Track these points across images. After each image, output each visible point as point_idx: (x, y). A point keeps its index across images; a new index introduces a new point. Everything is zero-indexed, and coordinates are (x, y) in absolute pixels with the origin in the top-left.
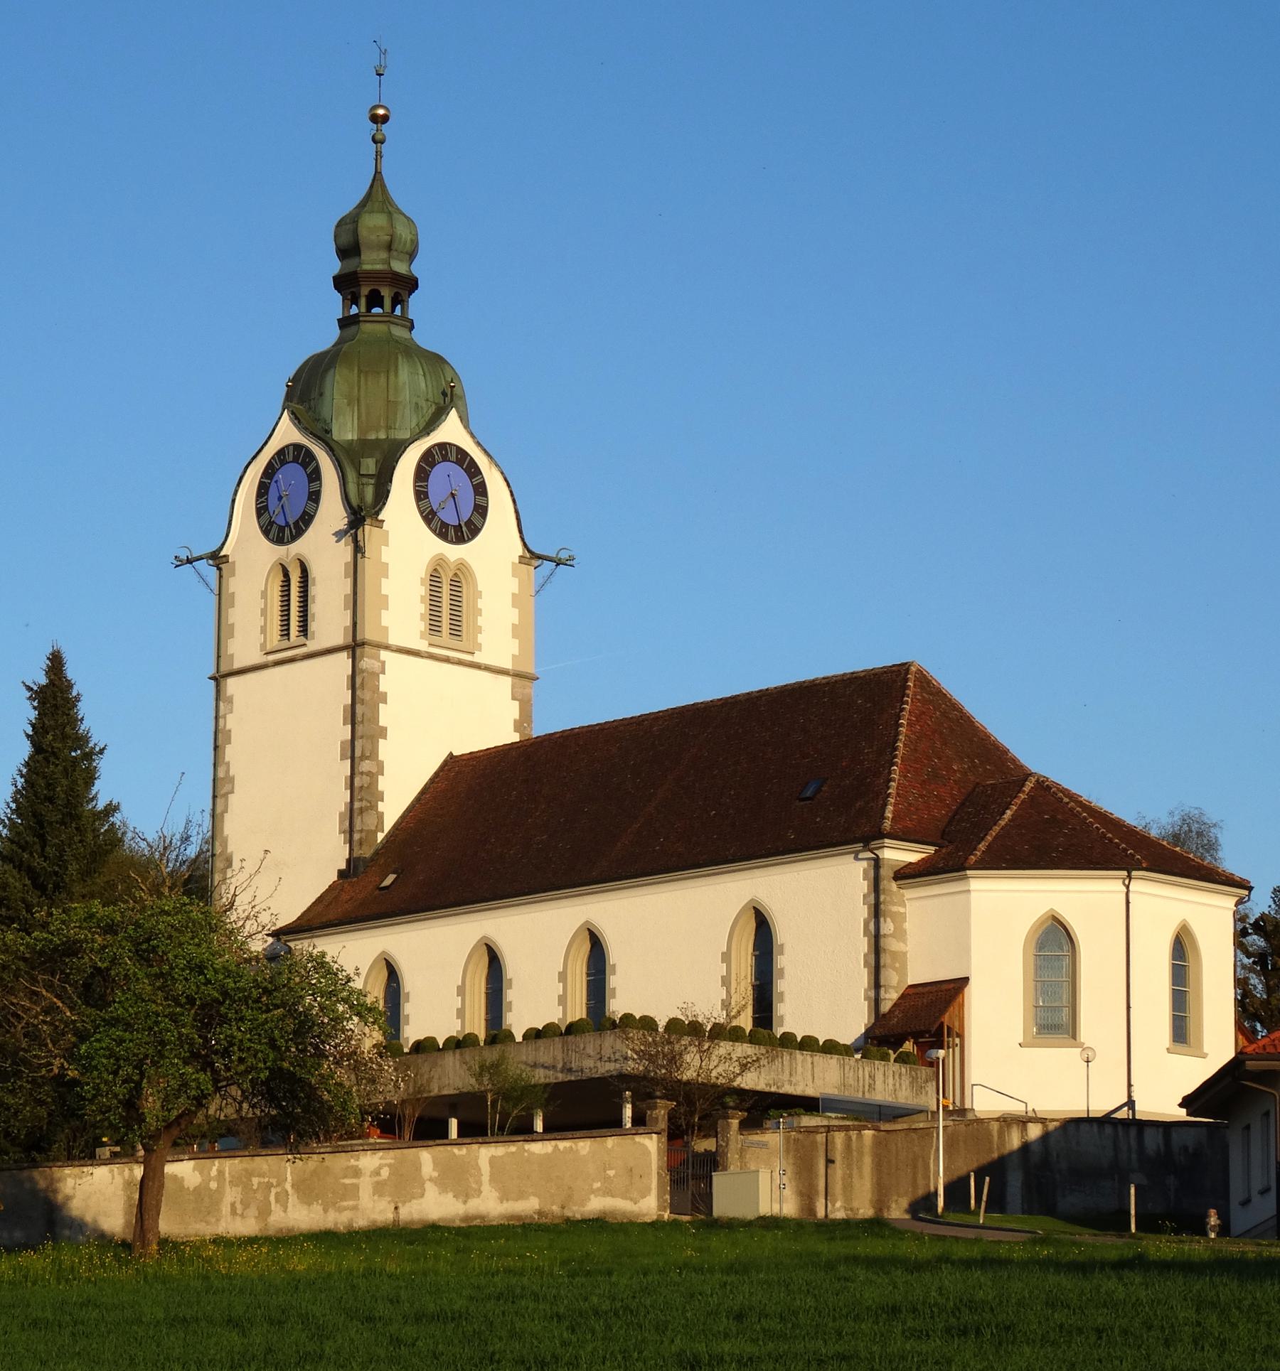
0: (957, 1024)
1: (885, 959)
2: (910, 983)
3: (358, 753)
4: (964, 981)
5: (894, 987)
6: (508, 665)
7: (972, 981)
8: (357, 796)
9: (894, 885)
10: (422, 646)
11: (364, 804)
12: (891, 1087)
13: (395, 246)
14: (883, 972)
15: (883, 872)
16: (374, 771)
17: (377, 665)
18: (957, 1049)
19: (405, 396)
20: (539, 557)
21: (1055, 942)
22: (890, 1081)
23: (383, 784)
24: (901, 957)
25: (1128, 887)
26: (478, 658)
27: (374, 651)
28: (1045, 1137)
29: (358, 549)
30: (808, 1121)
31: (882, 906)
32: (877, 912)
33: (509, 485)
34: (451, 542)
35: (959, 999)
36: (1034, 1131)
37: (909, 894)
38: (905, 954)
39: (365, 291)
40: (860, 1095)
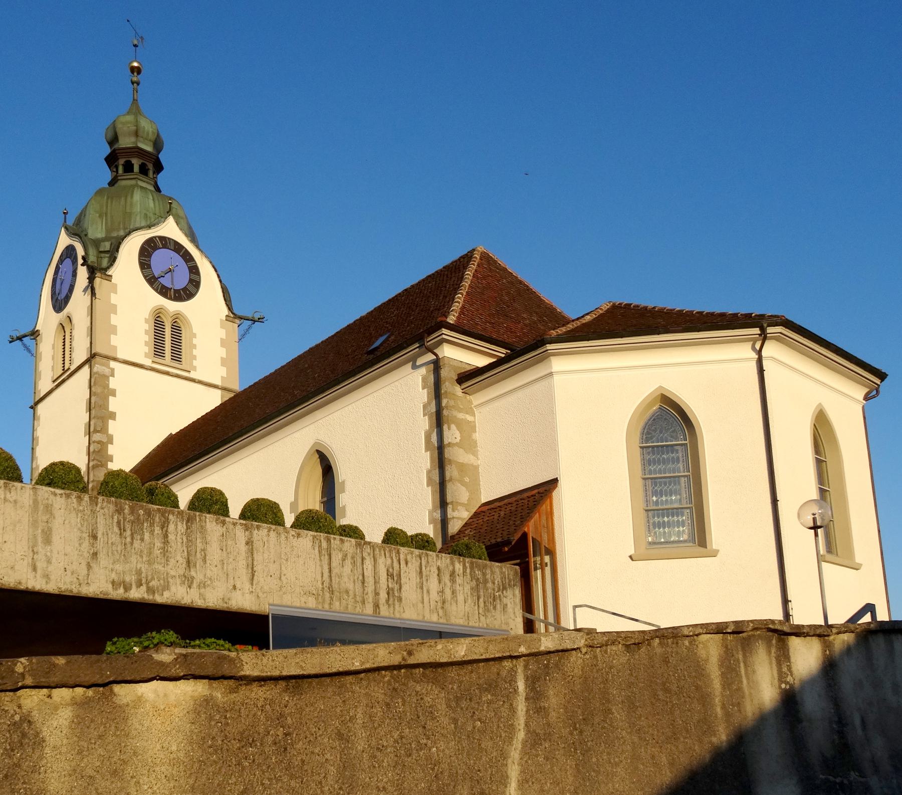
1: (451, 472)
2: (484, 500)
3: (92, 430)
5: (462, 504)
6: (218, 382)
7: (562, 483)
8: (92, 458)
9: (458, 390)
10: (148, 362)
11: (95, 462)
12: (434, 595)
13: (140, 133)
14: (450, 488)
15: (444, 373)
16: (105, 441)
17: (107, 371)
18: (548, 570)
19: (137, 208)
20: (241, 318)
21: (668, 429)
22: (433, 584)
23: (111, 450)
26: (192, 375)
27: (105, 360)
29: (93, 294)
30: (250, 661)
31: (445, 412)
32: (439, 421)
33: (216, 271)
34: (170, 299)
35: (544, 508)
36: (806, 658)
37: (477, 399)
38: (476, 468)
39: (121, 161)
40: (369, 609)
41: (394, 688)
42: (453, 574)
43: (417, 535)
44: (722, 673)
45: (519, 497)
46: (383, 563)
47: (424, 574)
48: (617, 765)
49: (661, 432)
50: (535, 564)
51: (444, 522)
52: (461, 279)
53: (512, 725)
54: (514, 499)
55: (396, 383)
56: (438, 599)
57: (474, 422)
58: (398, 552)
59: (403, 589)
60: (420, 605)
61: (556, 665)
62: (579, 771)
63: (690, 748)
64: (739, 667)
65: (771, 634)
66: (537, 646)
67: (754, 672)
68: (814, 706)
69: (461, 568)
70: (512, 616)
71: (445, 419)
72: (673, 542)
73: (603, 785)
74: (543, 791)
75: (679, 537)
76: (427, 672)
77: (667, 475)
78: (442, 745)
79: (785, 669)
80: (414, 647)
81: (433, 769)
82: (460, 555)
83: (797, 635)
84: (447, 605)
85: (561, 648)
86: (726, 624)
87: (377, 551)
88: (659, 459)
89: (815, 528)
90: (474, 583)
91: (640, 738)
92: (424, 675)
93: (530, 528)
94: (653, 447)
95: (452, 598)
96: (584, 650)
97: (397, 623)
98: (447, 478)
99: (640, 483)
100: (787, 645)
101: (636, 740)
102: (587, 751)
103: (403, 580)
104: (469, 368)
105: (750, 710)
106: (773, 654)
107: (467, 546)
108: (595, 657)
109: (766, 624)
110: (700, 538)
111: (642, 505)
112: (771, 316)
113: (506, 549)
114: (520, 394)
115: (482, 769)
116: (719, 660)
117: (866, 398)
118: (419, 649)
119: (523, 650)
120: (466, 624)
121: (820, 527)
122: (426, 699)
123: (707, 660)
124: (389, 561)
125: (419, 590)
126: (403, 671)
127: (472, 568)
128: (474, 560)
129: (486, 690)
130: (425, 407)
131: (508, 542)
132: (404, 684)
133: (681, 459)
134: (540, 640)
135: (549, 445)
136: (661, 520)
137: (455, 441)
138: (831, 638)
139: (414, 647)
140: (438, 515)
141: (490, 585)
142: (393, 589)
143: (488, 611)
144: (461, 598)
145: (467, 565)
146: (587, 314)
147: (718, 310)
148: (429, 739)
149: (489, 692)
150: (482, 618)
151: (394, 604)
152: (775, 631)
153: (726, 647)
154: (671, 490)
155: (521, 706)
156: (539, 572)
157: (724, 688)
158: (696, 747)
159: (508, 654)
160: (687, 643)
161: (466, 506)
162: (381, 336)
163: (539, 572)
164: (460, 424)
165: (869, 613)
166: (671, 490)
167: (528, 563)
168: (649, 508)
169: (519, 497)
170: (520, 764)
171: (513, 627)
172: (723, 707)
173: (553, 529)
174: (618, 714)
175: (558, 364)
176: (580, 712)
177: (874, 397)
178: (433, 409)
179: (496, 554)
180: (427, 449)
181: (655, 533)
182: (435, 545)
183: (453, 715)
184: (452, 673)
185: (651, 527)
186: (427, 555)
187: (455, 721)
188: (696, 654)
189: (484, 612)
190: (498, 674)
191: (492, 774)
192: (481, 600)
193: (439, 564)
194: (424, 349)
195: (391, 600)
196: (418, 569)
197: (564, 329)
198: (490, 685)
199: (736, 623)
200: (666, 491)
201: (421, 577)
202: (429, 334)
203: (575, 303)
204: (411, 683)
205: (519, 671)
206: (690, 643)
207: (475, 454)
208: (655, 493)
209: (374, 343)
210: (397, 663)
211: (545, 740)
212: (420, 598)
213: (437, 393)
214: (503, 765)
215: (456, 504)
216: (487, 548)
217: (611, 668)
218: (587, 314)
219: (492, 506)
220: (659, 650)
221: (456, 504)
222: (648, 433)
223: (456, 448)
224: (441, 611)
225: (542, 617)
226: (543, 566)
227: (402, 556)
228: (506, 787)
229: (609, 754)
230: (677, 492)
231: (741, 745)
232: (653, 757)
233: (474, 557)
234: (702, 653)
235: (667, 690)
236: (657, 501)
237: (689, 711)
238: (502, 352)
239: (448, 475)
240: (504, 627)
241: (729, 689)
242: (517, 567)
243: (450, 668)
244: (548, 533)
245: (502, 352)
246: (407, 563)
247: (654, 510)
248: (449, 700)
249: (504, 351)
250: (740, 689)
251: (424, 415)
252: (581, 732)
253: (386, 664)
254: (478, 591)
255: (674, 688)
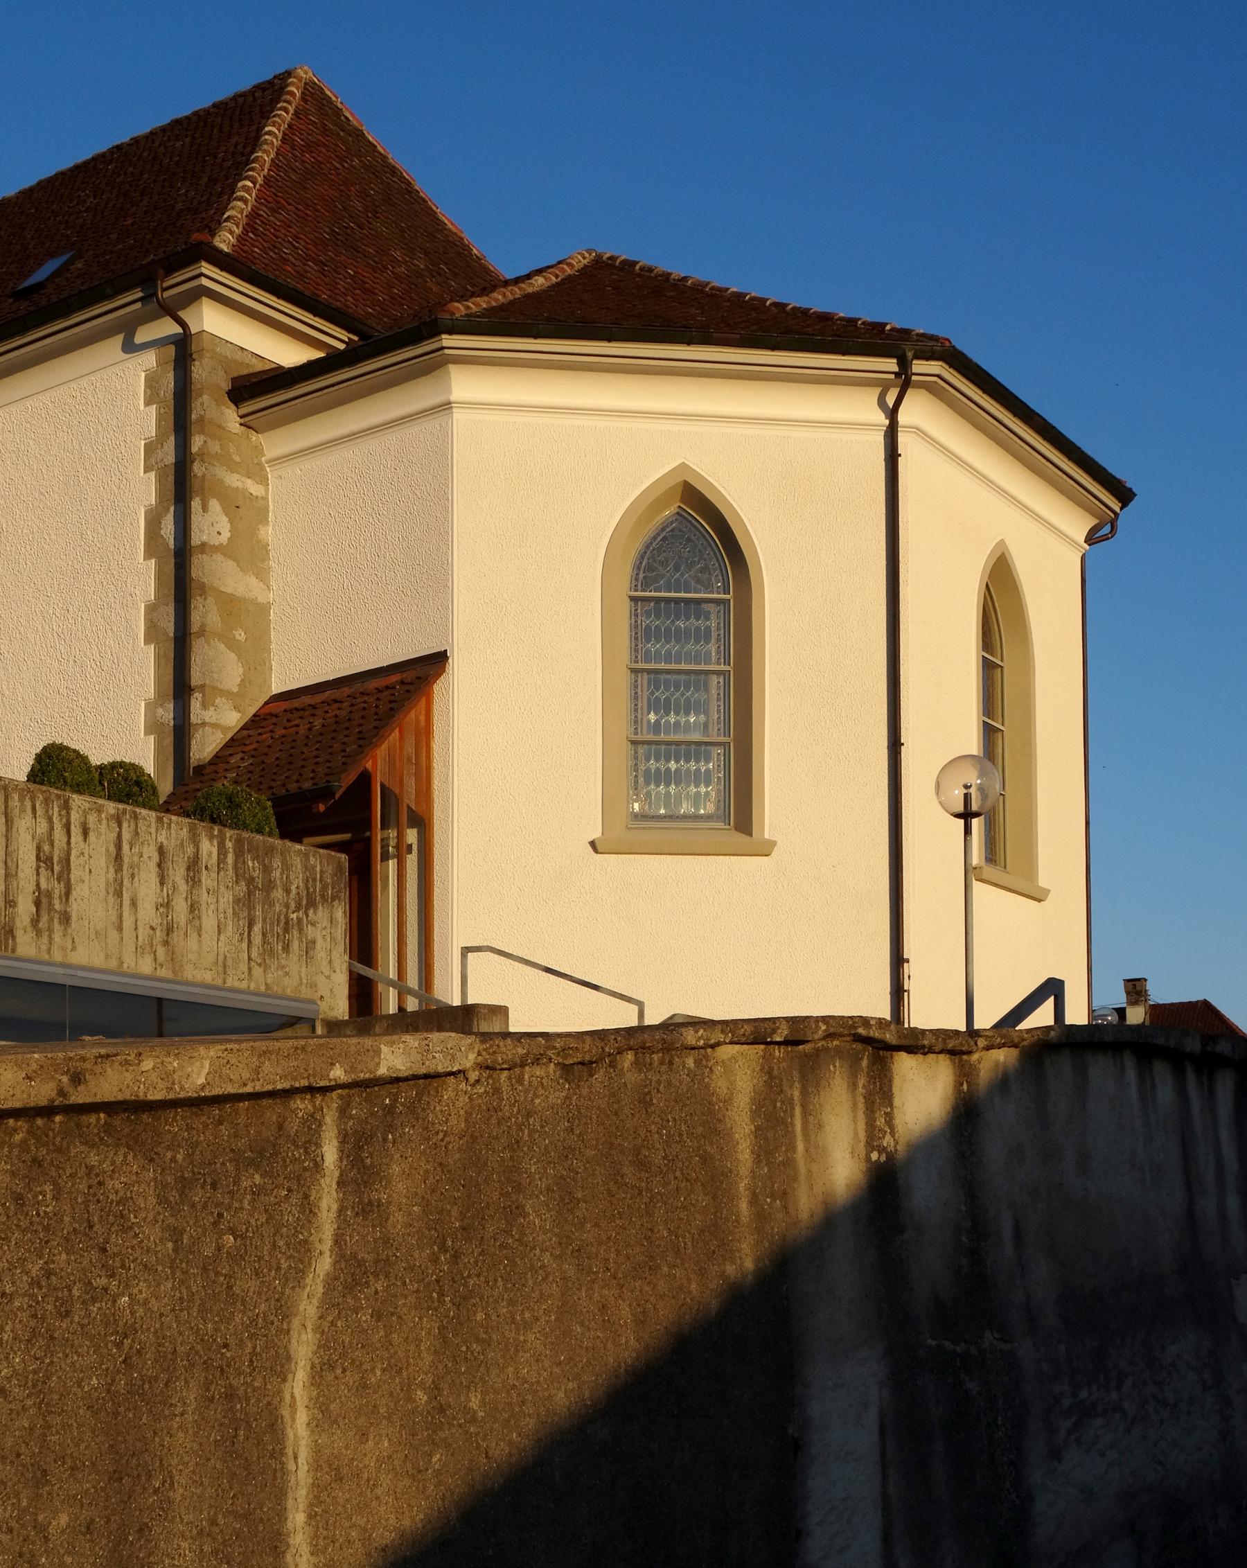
0: (410, 784)
1: (204, 613)
2: (276, 688)
4: (436, 662)
7: (458, 667)
9: (231, 417)
12: (148, 913)
14: (200, 653)
15: (200, 371)
18: (412, 861)
21: (690, 563)
22: (147, 887)
24: (252, 616)
25: (892, 414)
28: (966, 1114)
31: (197, 469)
32: (181, 486)
35: (413, 716)
36: (923, 1097)
37: (275, 444)
38: (264, 609)
41: (34, 1160)
42: (193, 865)
43: (114, 766)
44: (758, 1128)
45: (358, 687)
46: (27, 830)
47: (126, 860)
48: (527, 1326)
49: (677, 569)
50: (385, 847)
51: (181, 733)
52: (254, 141)
53: (306, 1241)
54: (346, 691)
55: (84, 382)
56: (156, 921)
57: (265, 499)
58: (66, 807)
59: (74, 894)
60: (113, 935)
61: (411, 1109)
62: (445, 1340)
63: (680, 1288)
64: (792, 1116)
65: (858, 1046)
66: (372, 1065)
67: (820, 1126)
68: (928, 1196)
69: (215, 851)
70: (324, 967)
71: (196, 485)
72: (685, 817)
73: (495, 1372)
74: (366, 1387)
75: (697, 806)
76: (117, 1121)
77: (683, 666)
78: (142, 1289)
79: (880, 1122)
80: (88, 1065)
81: (119, 1345)
82: (213, 820)
83: (910, 1050)
84: (176, 937)
85: (423, 1071)
86: (772, 1022)
87: (15, 801)
88: (668, 630)
89: (966, 815)
90: (242, 888)
91: (580, 1268)
92: (108, 1128)
93: (378, 763)
94: (658, 600)
95: (190, 921)
96: (473, 1076)
97: (57, 975)
98: (195, 628)
99: (623, 679)
100: (890, 1070)
101: (570, 1270)
102: (465, 1298)
103: (75, 873)
104: (259, 367)
105: (806, 1205)
106: (861, 1090)
107: (230, 799)
108: (497, 1090)
109: (853, 1027)
110: (740, 813)
111: (623, 729)
112: (923, 335)
113: (322, 808)
114: (373, 444)
115: (232, 1341)
116: (753, 1101)
117: (1091, 539)
118: (98, 1069)
119: (338, 1073)
120: (219, 982)
121: (977, 815)
122: (110, 1184)
123: (728, 1101)
124: (42, 827)
125: (111, 899)
126: (58, 1119)
127: (239, 853)
128: (245, 835)
129: (251, 1163)
130: (149, 449)
131: (327, 793)
132: (59, 1150)
133: (714, 634)
134: (378, 1052)
135: (432, 574)
136: (662, 765)
137: (216, 541)
138: (975, 1057)
139: (88, 1065)
140: (167, 714)
141: (278, 894)
142: (49, 894)
143: (272, 953)
144: (209, 921)
145: (229, 845)
146: (539, 272)
147: (818, 305)
148: (112, 1276)
149: (257, 1168)
150: (257, 971)
151: (50, 930)
152: (867, 1040)
153: (770, 1073)
154: (688, 701)
155: (328, 1200)
156: (392, 864)
157: (757, 1161)
158: (694, 1286)
159: (305, 1083)
160: (690, 1062)
161: (236, 700)
162: (52, 257)
163: (392, 864)
164: (234, 504)
165: (1051, 1000)
166: (688, 701)
167: (368, 843)
168: (639, 737)
169: (358, 687)
170: (318, 1329)
171: (326, 994)
172: (754, 1200)
173: (429, 769)
174: (538, 1215)
175: (464, 385)
176: (455, 1212)
177: (1105, 538)
178: (168, 454)
179: (295, 820)
180: (148, 554)
181: (648, 794)
182: (154, 790)
183: (171, 1220)
184: (175, 1124)
185: (641, 780)
186: (135, 817)
187: (176, 1234)
188: (707, 1087)
189: (262, 955)
190: (280, 1127)
191: (254, 1353)
192: (257, 929)
193: (162, 838)
194: (153, 306)
195: (44, 918)
196: (112, 849)
197: (483, 302)
198: (261, 1153)
199: (793, 1021)
200: (677, 701)
201: (119, 869)
202: (170, 271)
203: (518, 243)
204: (77, 1148)
205: (328, 1120)
206: (698, 1062)
207: (263, 575)
208: (654, 705)
209: (31, 272)
210: (43, 1102)
211: (376, 1276)
212: (114, 918)
213: (180, 417)
214: (280, 1331)
215: (212, 693)
216: (277, 802)
217: (529, 1115)
218: (539, 272)
219: (296, 703)
220: (632, 1078)
221: (212, 693)
222: (650, 568)
223: (219, 557)
224: (161, 951)
225: (393, 974)
226: (402, 851)
227: (75, 817)
228: (284, 1380)
229: (512, 1302)
230: (701, 708)
231: (785, 1270)
232: (604, 1308)
233: (245, 827)
234: (720, 1084)
235: (642, 1165)
236: (657, 722)
237: (684, 1208)
238: (338, 338)
239: (196, 619)
240: (305, 993)
241: (768, 1163)
242: (344, 857)
243: (171, 1114)
244: (417, 775)
245: (338, 338)
246: (85, 833)
247: (649, 743)
248: (165, 1186)
249: (344, 335)
250: (789, 1163)
251: (147, 469)
252: (456, 1257)
253: (18, 1105)
254: (251, 908)
255: (657, 1159)
